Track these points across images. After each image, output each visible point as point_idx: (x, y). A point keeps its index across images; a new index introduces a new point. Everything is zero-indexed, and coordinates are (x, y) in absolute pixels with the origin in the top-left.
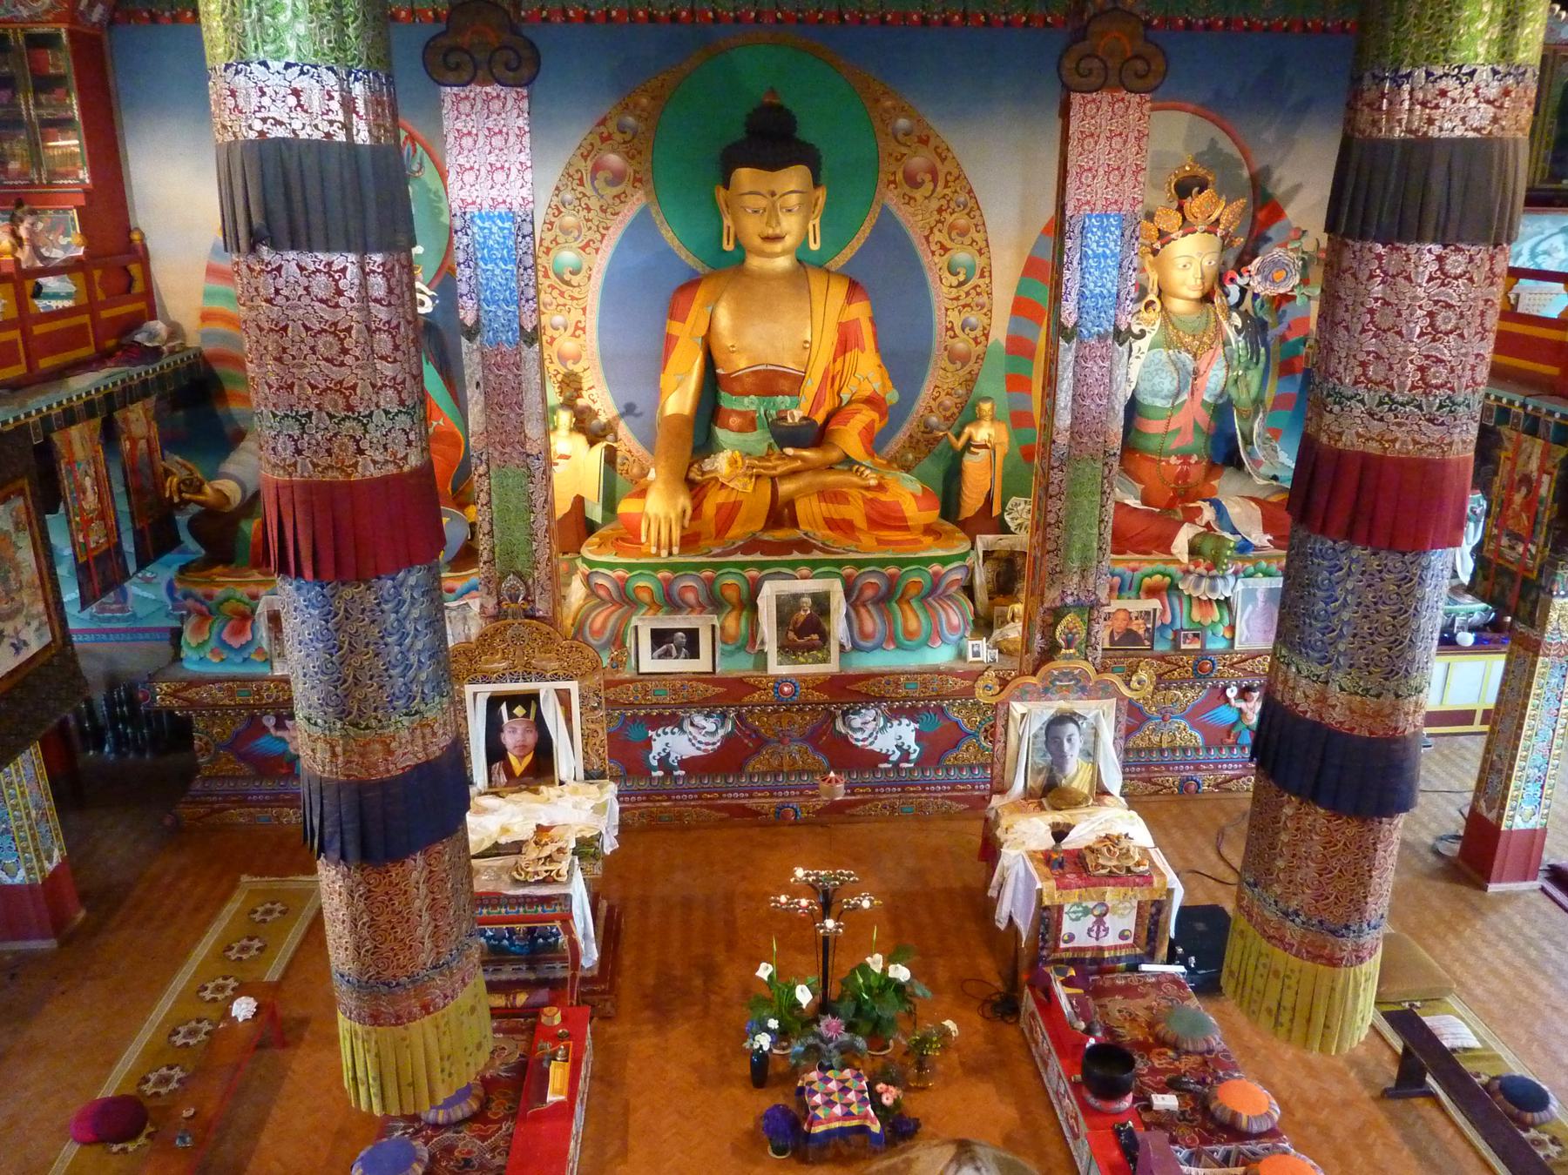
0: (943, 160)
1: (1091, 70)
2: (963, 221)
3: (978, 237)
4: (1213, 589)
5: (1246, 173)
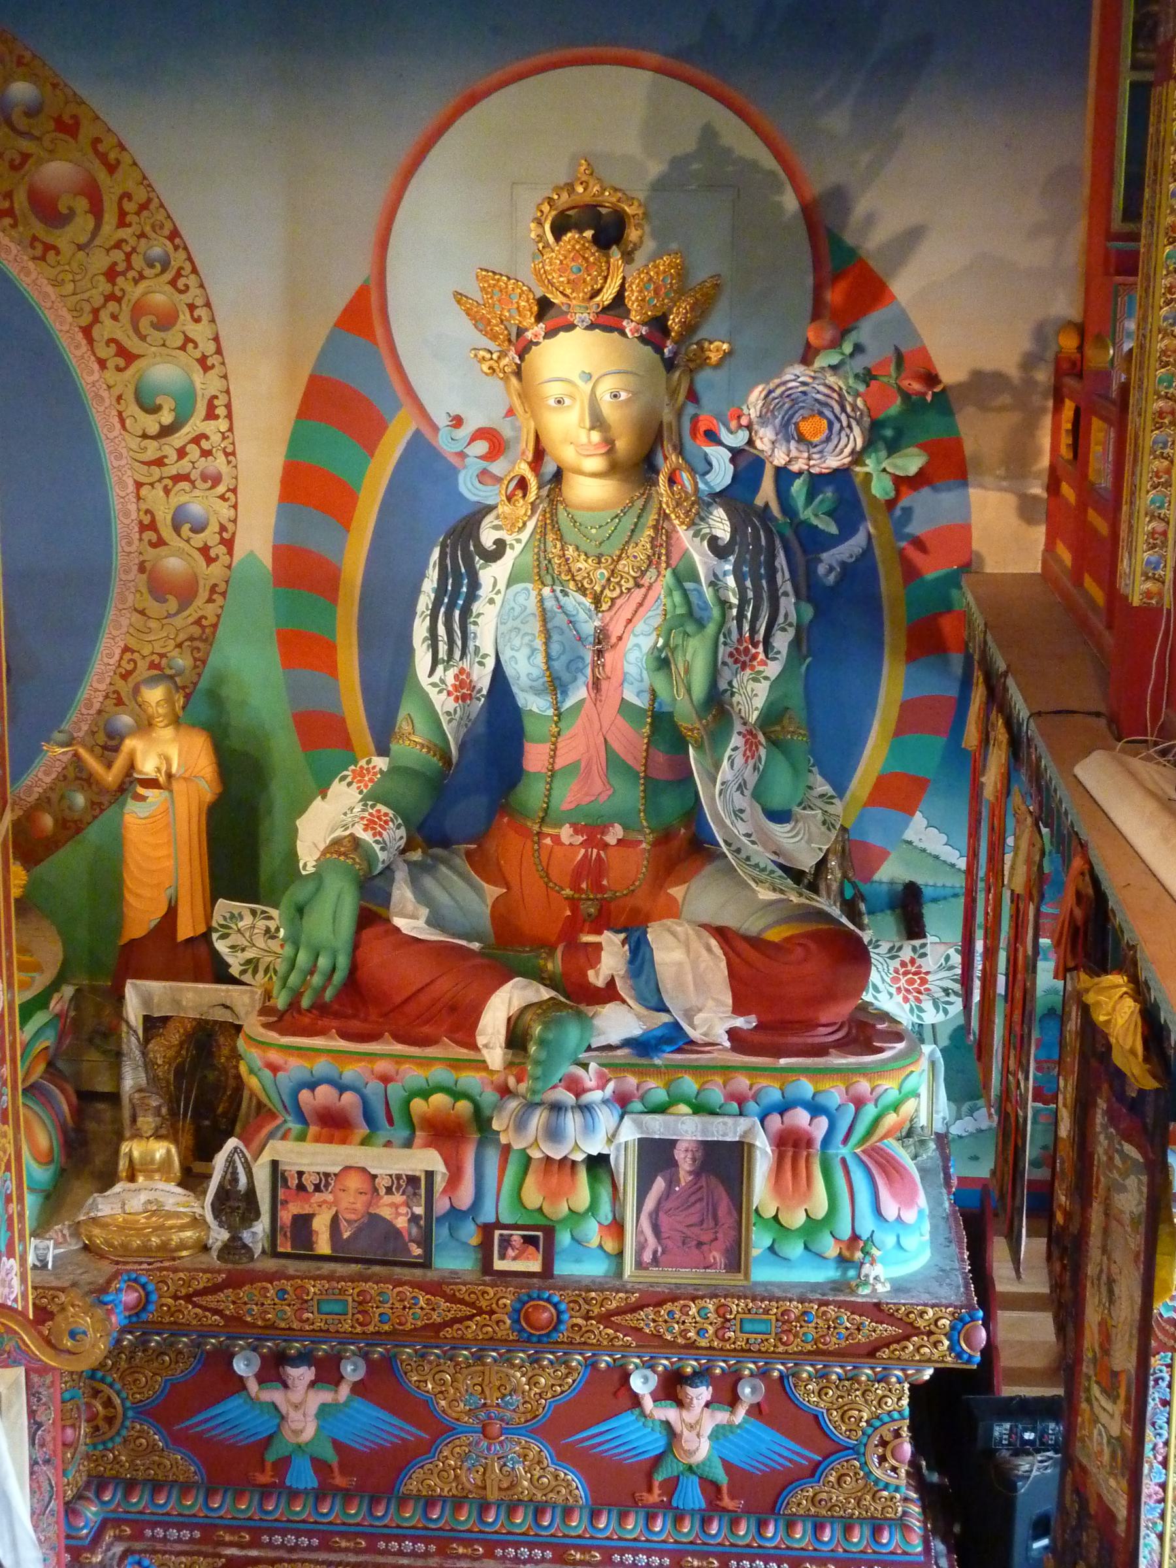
0: (112, 168)
2: (160, 296)
4: (554, 1134)
5: (790, 202)
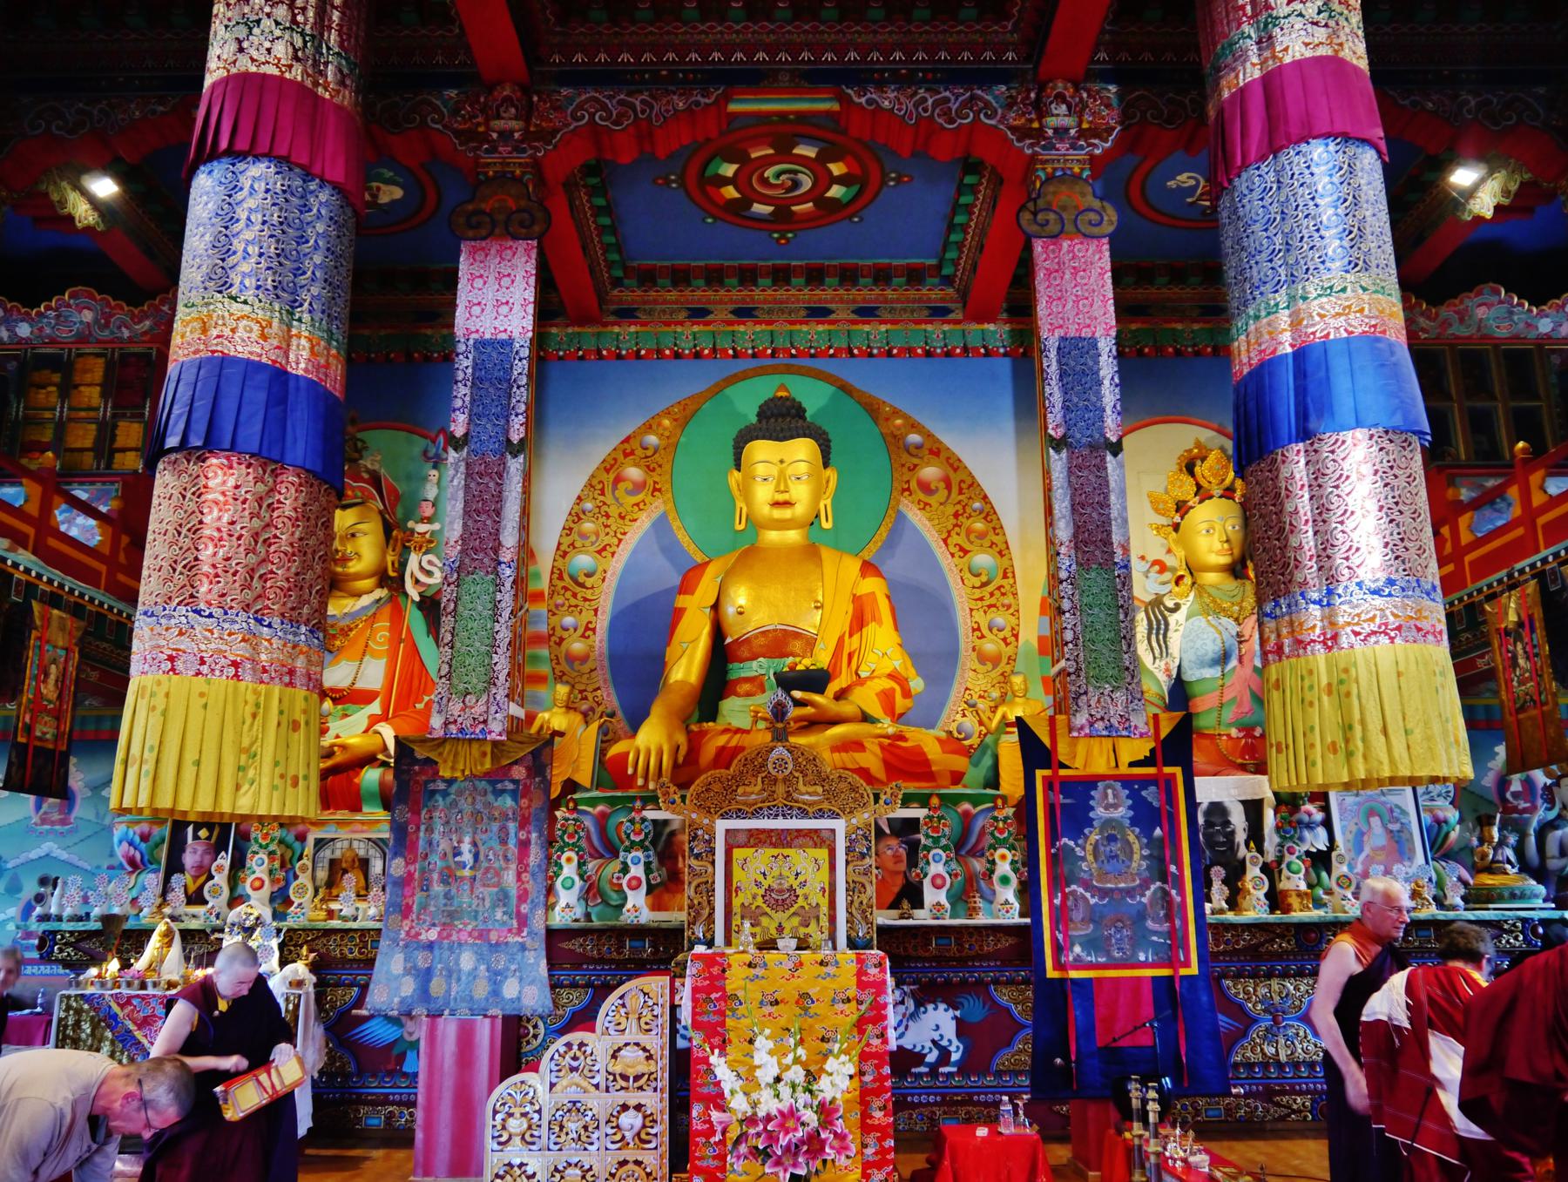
0: (955, 470)
1: (1047, 222)
3: (996, 539)
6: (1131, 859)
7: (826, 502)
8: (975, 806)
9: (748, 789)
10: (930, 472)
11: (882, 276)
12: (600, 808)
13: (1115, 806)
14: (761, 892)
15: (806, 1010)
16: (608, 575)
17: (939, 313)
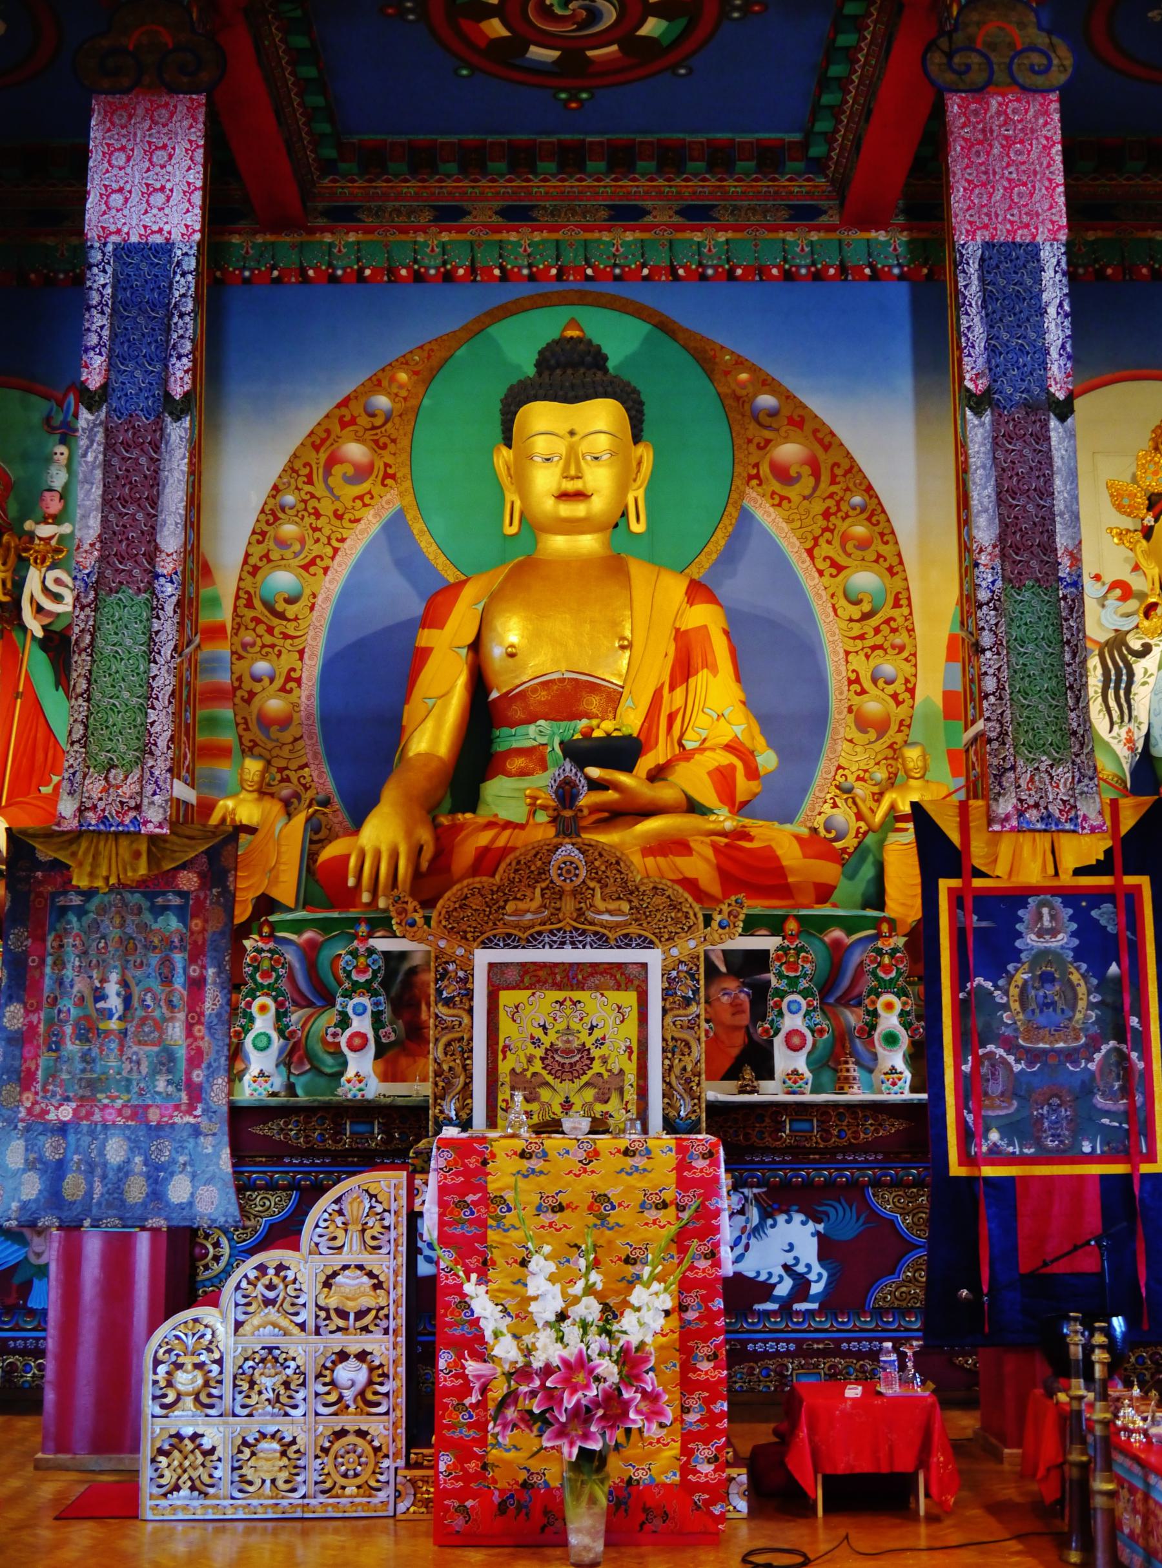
3: (884, 550)
6: (1074, 1007)
7: (636, 494)
8: (849, 934)
9: (522, 905)
10: (789, 451)
11: (721, 159)
12: (307, 935)
13: (1053, 932)
14: (539, 1052)
15: (603, 1218)
16: (319, 601)
17: (804, 215)
